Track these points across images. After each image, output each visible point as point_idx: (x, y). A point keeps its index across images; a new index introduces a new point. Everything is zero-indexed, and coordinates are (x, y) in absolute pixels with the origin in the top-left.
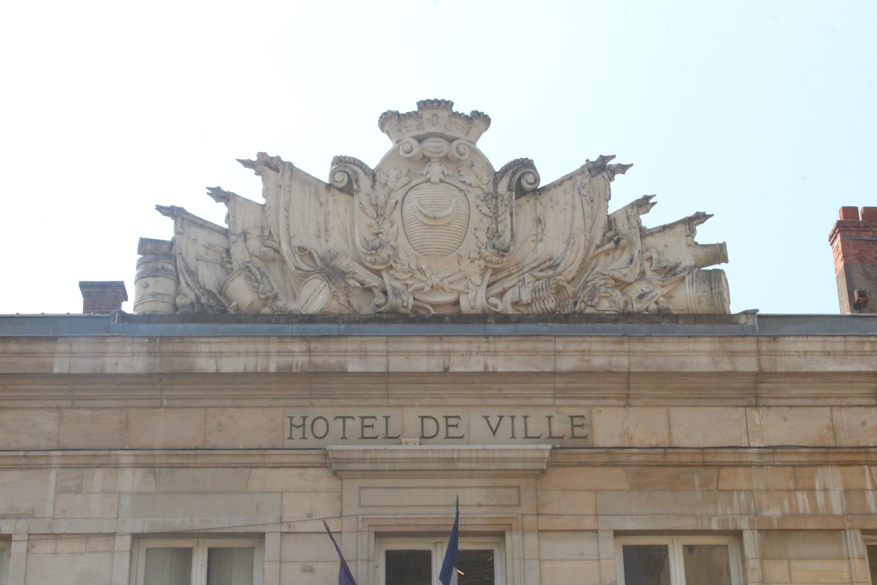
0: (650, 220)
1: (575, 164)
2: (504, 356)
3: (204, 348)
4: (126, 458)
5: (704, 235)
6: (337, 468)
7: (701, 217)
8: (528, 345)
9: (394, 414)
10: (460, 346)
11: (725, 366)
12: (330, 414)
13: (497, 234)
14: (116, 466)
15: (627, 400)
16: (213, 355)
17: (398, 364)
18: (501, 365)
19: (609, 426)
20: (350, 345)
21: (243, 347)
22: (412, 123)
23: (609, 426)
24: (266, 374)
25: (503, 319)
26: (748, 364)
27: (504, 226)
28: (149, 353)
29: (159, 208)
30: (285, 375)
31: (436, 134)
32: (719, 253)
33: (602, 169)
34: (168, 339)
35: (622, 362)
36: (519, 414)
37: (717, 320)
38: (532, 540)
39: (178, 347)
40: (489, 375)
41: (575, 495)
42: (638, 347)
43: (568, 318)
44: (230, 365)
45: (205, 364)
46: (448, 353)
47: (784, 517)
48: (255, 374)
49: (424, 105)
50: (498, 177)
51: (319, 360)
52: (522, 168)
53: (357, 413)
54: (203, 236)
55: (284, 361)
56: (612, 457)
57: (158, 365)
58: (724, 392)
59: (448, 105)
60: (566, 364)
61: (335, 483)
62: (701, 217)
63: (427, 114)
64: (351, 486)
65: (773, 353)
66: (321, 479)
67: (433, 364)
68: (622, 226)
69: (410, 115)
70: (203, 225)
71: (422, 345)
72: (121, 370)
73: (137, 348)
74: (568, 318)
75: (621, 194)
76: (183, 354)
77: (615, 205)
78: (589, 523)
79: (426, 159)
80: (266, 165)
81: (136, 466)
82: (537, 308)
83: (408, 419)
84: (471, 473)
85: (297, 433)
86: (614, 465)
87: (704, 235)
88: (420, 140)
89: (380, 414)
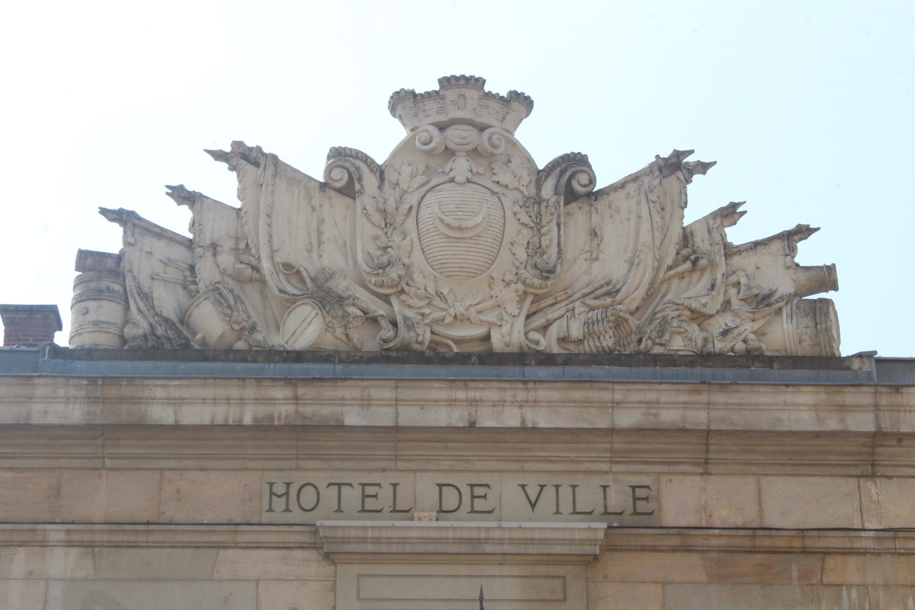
0: (737, 235)
2: (549, 407)
3: (160, 393)
4: (56, 534)
5: (808, 254)
6: (330, 551)
7: (804, 232)
8: (578, 394)
9: (404, 481)
10: (490, 393)
11: (833, 425)
12: (321, 479)
13: (539, 250)
14: (43, 544)
15: (705, 466)
16: (169, 401)
17: (410, 416)
18: (543, 419)
19: (683, 499)
20: (348, 391)
21: (209, 393)
22: (432, 105)
23: (683, 499)
24: (240, 427)
25: (547, 359)
26: (863, 422)
27: (550, 240)
28: (91, 400)
29: (104, 212)
30: (263, 429)
31: (462, 120)
32: (826, 278)
33: (676, 168)
34: (108, 380)
35: (699, 418)
36: (566, 482)
37: (822, 364)
39: (126, 391)
40: (527, 432)
42: (721, 398)
43: (631, 359)
44: (193, 415)
45: (162, 415)
46: (473, 403)
48: (225, 427)
49: (446, 82)
50: (541, 176)
51: (308, 410)
52: (573, 165)
53: (356, 478)
54: (160, 248)
55: (263, 410)
56: (685, 539)
57: (100, 415)
58: (831, 457)
60: (627, 419)
61: (326, 570)
62: (804, 232)
63: (451, 95)
64: (348, 573)
65: (896, 408)
66: (308, 564)
67: (456, 417)
68: (701, 242)
69: (429, 95)
70: (160, 233)
71: (440, 392)
72: (52, 420)
73: (73, 392)
74: (631, 359)
75: (701, 200)
76: (133, 400)
77: (692, 215)
79: (449, 153)
80: (243, 158)
81: (70, 544)
82: (590, 346)
83: (422, 487)
84: (503, 558)
85: (279, 504)
86: (688, 550)
87: (808, 254)
88: (442, 127)
89: (386, 480)
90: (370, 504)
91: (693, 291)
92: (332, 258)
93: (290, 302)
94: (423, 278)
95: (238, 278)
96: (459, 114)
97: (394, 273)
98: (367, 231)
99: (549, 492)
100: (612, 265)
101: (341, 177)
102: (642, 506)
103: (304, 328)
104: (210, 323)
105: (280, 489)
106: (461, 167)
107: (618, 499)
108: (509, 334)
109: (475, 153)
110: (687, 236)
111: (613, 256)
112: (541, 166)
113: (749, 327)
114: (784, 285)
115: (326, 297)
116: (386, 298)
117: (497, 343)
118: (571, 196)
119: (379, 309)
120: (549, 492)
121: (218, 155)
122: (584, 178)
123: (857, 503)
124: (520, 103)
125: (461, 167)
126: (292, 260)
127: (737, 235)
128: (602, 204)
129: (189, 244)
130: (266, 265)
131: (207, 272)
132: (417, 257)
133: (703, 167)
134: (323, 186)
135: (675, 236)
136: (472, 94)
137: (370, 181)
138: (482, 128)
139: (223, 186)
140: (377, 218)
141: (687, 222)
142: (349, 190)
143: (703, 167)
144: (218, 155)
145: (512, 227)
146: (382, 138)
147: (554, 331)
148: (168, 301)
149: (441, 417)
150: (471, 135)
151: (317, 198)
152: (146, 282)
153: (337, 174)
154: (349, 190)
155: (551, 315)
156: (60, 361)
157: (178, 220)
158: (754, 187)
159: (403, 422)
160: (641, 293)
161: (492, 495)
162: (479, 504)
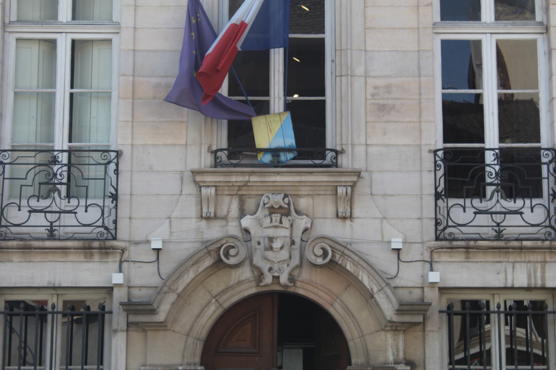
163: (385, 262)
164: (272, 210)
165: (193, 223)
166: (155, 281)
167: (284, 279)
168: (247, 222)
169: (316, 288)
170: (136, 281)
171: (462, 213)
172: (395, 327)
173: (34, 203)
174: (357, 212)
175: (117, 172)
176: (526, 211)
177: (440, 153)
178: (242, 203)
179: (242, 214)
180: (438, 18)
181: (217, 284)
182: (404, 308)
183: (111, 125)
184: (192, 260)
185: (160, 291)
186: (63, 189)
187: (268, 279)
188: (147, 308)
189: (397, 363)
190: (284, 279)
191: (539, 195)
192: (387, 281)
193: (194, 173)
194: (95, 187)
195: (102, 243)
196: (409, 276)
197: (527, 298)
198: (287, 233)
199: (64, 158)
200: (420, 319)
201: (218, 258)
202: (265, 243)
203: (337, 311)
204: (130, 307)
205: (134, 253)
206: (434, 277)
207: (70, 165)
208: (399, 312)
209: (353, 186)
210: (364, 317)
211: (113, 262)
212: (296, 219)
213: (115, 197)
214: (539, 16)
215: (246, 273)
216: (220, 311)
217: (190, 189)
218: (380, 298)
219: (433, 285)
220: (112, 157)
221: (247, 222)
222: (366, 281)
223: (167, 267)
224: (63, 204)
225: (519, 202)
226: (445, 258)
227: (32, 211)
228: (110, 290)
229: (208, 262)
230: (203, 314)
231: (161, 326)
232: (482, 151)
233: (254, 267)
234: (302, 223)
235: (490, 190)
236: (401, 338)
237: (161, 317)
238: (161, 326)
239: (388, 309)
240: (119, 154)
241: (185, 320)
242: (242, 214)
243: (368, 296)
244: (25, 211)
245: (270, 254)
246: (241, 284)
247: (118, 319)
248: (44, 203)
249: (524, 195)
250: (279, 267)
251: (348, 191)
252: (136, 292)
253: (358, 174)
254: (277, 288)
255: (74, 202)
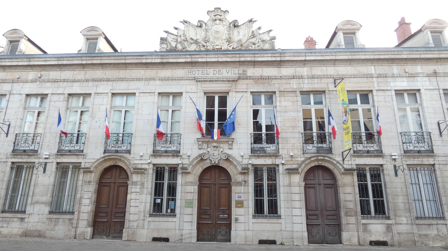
0: (261, 31)
1: (246, 20)
5: (272, 34)
7: (271, 31)
9: (208, 70)
36: (233, 69)
37: (273, 50)
38: (234, 93)
41: (242, 85)
47: (284, 89)
49: (215, 9)
50: (230, 24)
53: (201, 70)
54: (173, 36)
56: (250, 78)
59: (220, 9)
62: (271, 31)
63: (216, 10)
68: (255, 33)
69: (212, 11)
78: (245, 90)
79: (216, 20)
82: (237, 49)
85: (189, 74)
87: (272, 34)
88: (215, 16)
90: (203, 73)
91: (253, 40)
92: (198, 37)
93: (192, 43)
94: (212, 39)
95: (184, 41)
96: (217, 14)
97: (207, 39)
98: (203, 33)
99: (230, 71)
100: (241, 37)
101: (199, 24)
102: (244, 73)
103: (193, 47)
104: (180, 47)
105: (190, 71)
106: (218, 22)
107: (241, 72)
108: (225, 47)
109: (220, 20)
110: (253, 32)
111: (241, 36)
112: (230, 22)
113: (262, 45)
114: (268, 39)
115: (196, 42)
116: (206, 43)
117: (223, 49)
118: (235, 26)
119: (205, 44)
120: (230, 71)
121: (181, 22)
122: (237, 23)
123: (441, 225)
124: (226, 11)
125: (218, 22)
126: (192, 37)
127: (261, 31)
128: (240, 27)
129: (177, 36)
130: (188, 38)
131: (179, 40)
132: (211, 36)
133: (256, 21)
134: (197, 26)
135: (251, 32)
136: (219, 10)
137: (204, 25)
138: (221, 16)
139: (182, 26)
140: (205, 31)
141: (253, 30)
142: (201, 26)
143: (256, 21)
144: (181, 22)
145: (226, 32)
146: (206, 18)
147: (232, 47)
148: (174, 44)
149: (213, 60)
150: (219, 17)
151: (196, 28)
152: (170, 41)
153: (199, 24)
154: (201, 26)
155: (231, 44)
156: (274, 91)
157: (175, 32)
158: (264, 23)
159: (208, 61)
160: (245, 41)
161: (221, 72)
162: (220, 73)
163: (240, 159)
164: (214, 147)
165: (197, 150)
166: (188, 163)
167: (217, 162)
168: (209, 150)
169: (224, 165)
170: (184, 163)
171: (360, 147)
172: (242, 173)
173: (162, 145)
174: (233, 147)
175: (180, 138)
176: (271, 147)
177: (252, 134)
178: (208, 145)
179: (208, 148)
180: (252, 104)
181: (201, 164)
182: (243, 169)
183: (180, 129)
184: (196, 158)
185: (189, 165)
186: (169, 142)
187: (213, 162)
188: (186, 169)
189: (242, 181)
190: (217, 162)
191: (275, 143)
192: (239, 163)
193: (197, 139)
194: (176, 142)
195: (176, 154)
196: (245, 162)
197: (272, 166)
198: (217, 152)
199: (169, 135)
200: (247, 171)
201: (201, 159)
202: (212, 154)
203: (229, 170)
204: (183, 168)
205: (184, 157)
206: (250, 162)
207: (171, 137)
208: (242, 170)
209: (233, 142)
210: (235, 171)
211: (179, 158)
212: (299, 175)
213: (180, 144)
214: (274, 104)
215: (208, 161)
216: (202, 170)
217: (197, 142)
218: (238, 167)
219: (250, 164)
220: (179, 135)
221: (209, 150)
222: (235, 163)
223: (191, 159)
224: (168, 145)
225: (270, 145)
226: (253, 158)
227: (414, 147)
228: (178, 165)
229: (200, 159)
230: (199, 170)
231: (189, 173)
232: (262, 134)
233: (210, 160)
234: (221, 150)
235: (263, 142)
236: (243, 176)
237: (189, 171)
238: (189, 173)
239: (240, 169)
240: (181, 135)
241: (194, 172)
242: (208, 148)
243: (235, 166)
244: (160, 147)
245: (213, 157)
246: (207, 164)
247: (180, 171)
248: (164, 145)
249: (271, 143)
250: (215, 161)
251: (231, 143)
252: (184, 165)
253: (233, 139)
254: (215, 164)
255: (171, 145)
